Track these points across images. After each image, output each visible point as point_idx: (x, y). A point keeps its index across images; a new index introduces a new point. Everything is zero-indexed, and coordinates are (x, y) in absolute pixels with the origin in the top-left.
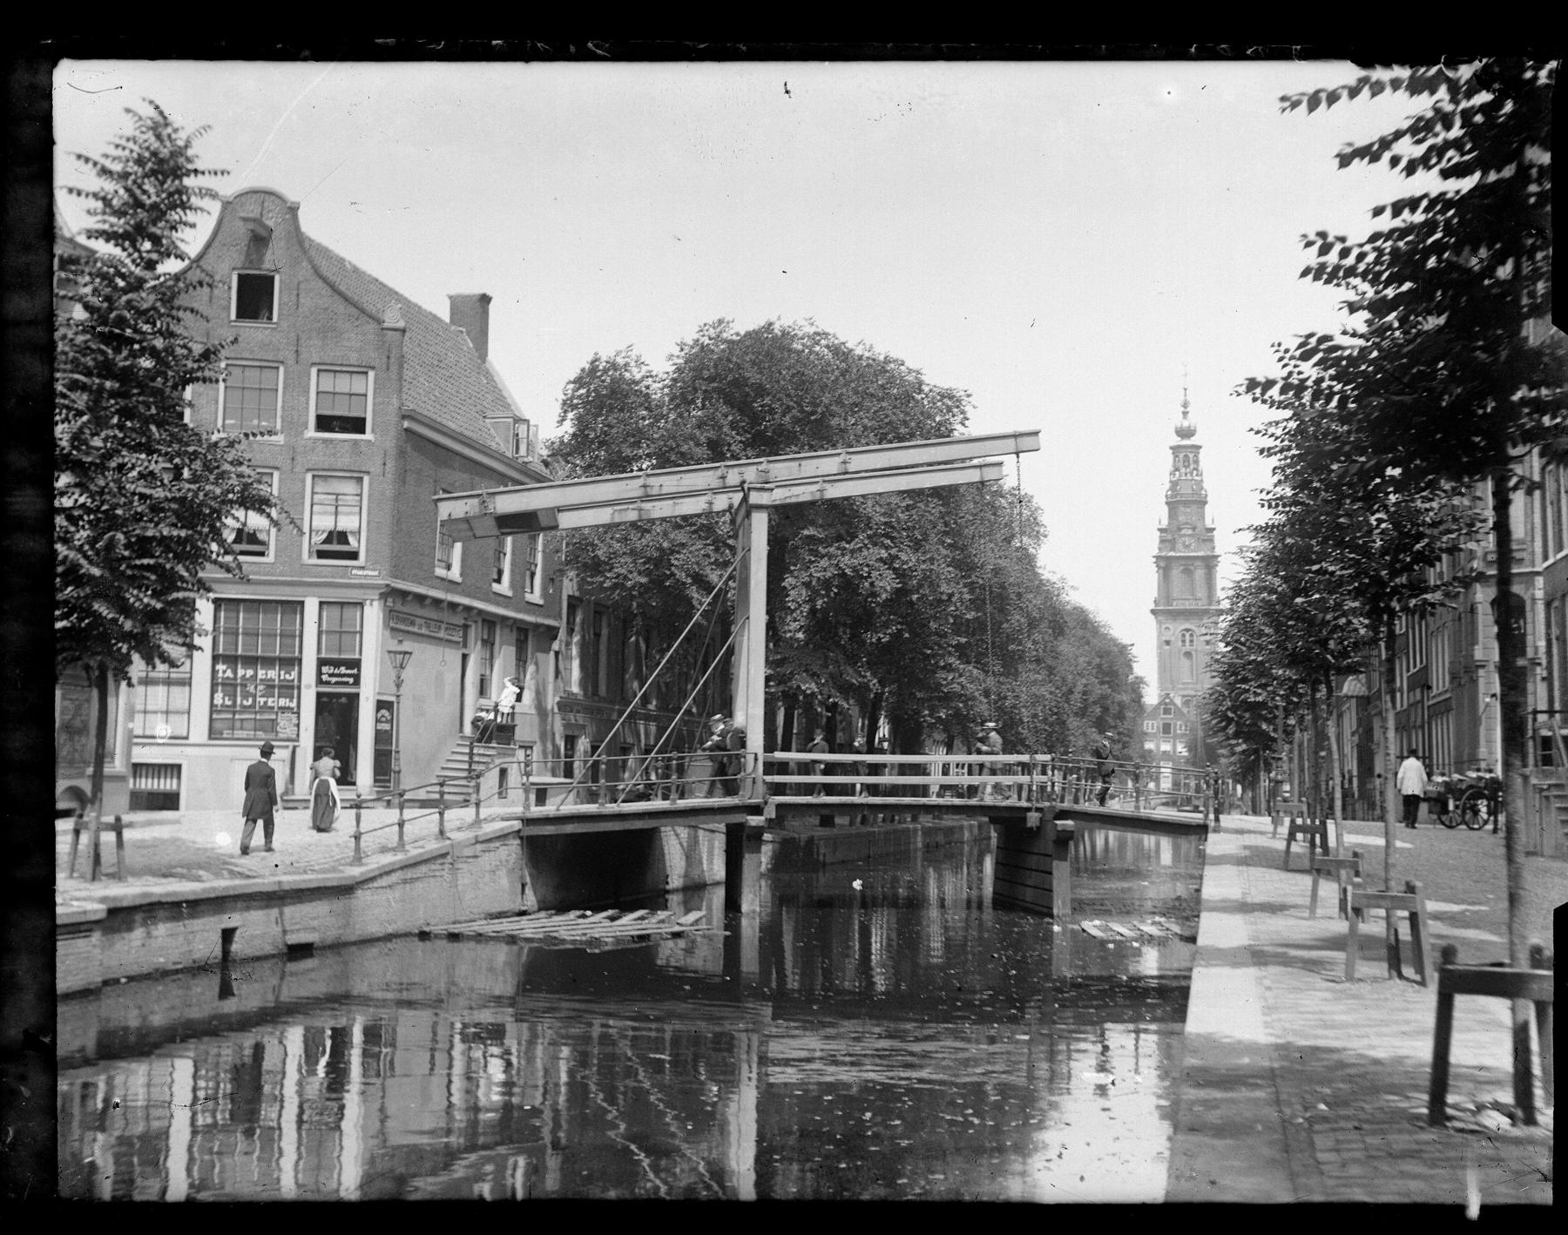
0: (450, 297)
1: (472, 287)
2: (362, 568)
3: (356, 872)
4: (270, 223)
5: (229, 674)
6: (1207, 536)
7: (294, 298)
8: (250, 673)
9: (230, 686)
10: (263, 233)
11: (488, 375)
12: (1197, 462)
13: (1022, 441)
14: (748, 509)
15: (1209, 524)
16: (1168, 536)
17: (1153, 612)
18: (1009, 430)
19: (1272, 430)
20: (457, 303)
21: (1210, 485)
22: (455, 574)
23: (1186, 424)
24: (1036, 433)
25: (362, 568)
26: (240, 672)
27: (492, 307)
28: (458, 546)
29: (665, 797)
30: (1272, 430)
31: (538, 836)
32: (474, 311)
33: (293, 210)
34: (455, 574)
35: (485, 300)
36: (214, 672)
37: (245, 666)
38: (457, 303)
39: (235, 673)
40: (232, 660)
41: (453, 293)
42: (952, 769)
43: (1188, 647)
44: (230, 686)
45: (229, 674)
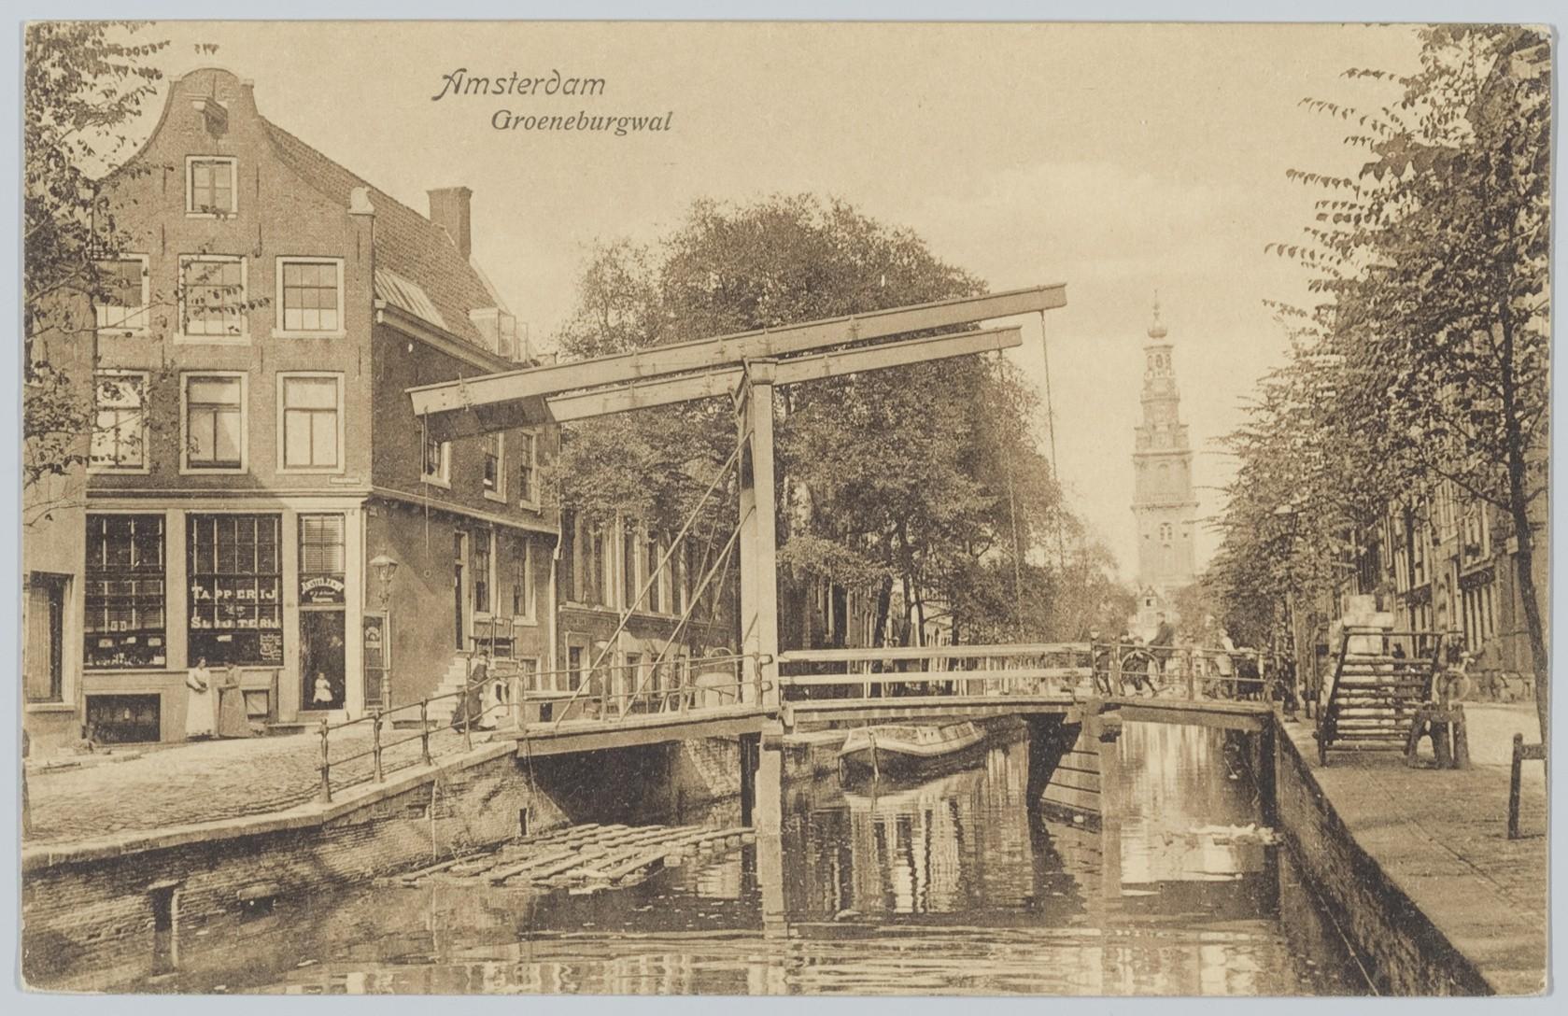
1: (451, 181)
2: (343, 476)
3: (315, 809)
4: (224, 104)
5: (206, 595)
6: (1178, 429)
8: (228, 593)
10: (218, 116)
12: (1169, 361)
16: (1147, 433)
22: (445, 480)
23: (1158, 324)
24: (1063, 286)
25: (343, 476)
26: (218, 593)
27: (472, 201)
28: (446, 446)
29: (674, 707)
31: (601, 752)
33: (249, 88)
34: (445, 480)
35: (465, 193)
36: (190, 594)
37: (222, 588)
40: (207, 582)
41: (431, 188)
42: (867, 690)
43: (1166, 541)
44: (205, 609)
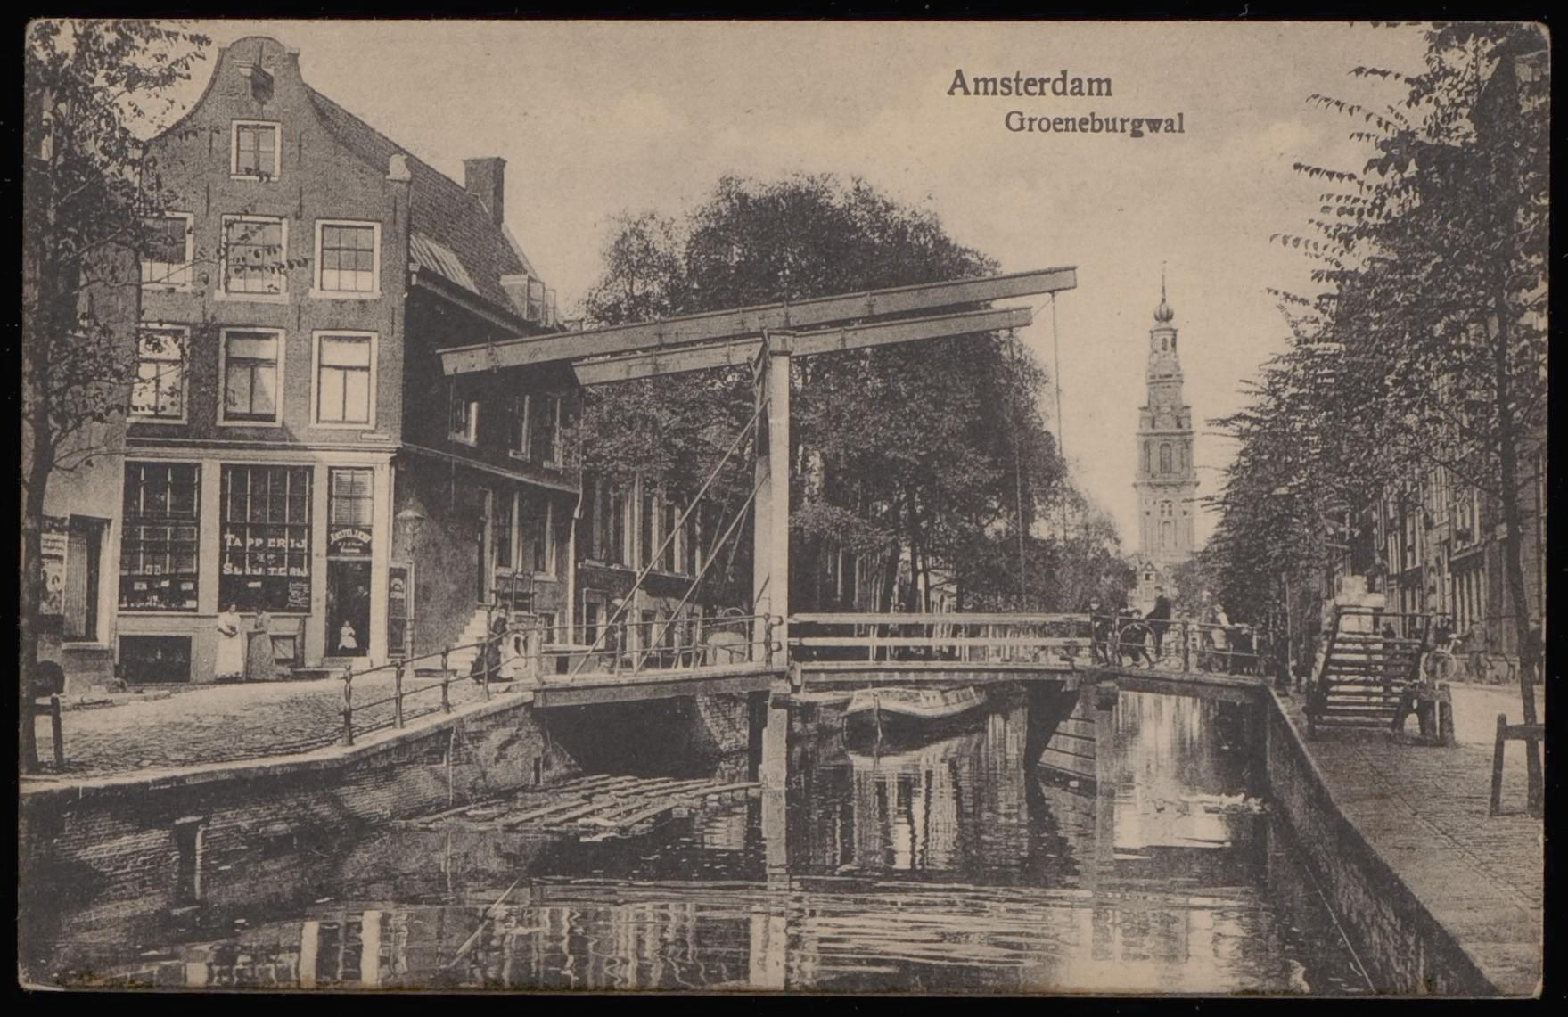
0: (465, 162)
2: (372, 432)
4: (270, 71)
5: (238, 543)
7: (295, 149)
8: (259, 542)
9: (237, 556)
11: (505, 242)
13: (1053, 281)
14: (766, 356)
15: (1185, 403)
17: (1135, 486)
18: (1030, 269)
19: (546, 774)
20: (473, 166)
21: (1187, 369)
24: (1074, 269)
26: (249, 542)
30: (546, 774)
32: (491, 173)
34: (472, 439)
35: (500, 163)
38: (473, 166)
39: (244, 541)
40: (239, 531)
43: (1166, 517)
44: (237, 556)
45: (238, 543)
